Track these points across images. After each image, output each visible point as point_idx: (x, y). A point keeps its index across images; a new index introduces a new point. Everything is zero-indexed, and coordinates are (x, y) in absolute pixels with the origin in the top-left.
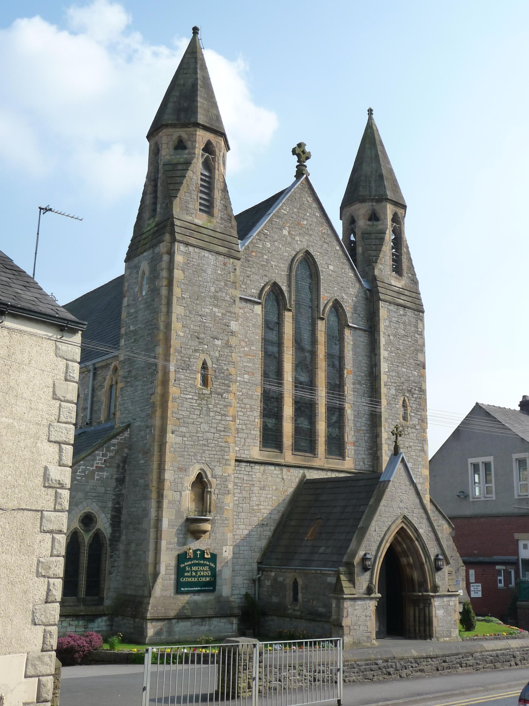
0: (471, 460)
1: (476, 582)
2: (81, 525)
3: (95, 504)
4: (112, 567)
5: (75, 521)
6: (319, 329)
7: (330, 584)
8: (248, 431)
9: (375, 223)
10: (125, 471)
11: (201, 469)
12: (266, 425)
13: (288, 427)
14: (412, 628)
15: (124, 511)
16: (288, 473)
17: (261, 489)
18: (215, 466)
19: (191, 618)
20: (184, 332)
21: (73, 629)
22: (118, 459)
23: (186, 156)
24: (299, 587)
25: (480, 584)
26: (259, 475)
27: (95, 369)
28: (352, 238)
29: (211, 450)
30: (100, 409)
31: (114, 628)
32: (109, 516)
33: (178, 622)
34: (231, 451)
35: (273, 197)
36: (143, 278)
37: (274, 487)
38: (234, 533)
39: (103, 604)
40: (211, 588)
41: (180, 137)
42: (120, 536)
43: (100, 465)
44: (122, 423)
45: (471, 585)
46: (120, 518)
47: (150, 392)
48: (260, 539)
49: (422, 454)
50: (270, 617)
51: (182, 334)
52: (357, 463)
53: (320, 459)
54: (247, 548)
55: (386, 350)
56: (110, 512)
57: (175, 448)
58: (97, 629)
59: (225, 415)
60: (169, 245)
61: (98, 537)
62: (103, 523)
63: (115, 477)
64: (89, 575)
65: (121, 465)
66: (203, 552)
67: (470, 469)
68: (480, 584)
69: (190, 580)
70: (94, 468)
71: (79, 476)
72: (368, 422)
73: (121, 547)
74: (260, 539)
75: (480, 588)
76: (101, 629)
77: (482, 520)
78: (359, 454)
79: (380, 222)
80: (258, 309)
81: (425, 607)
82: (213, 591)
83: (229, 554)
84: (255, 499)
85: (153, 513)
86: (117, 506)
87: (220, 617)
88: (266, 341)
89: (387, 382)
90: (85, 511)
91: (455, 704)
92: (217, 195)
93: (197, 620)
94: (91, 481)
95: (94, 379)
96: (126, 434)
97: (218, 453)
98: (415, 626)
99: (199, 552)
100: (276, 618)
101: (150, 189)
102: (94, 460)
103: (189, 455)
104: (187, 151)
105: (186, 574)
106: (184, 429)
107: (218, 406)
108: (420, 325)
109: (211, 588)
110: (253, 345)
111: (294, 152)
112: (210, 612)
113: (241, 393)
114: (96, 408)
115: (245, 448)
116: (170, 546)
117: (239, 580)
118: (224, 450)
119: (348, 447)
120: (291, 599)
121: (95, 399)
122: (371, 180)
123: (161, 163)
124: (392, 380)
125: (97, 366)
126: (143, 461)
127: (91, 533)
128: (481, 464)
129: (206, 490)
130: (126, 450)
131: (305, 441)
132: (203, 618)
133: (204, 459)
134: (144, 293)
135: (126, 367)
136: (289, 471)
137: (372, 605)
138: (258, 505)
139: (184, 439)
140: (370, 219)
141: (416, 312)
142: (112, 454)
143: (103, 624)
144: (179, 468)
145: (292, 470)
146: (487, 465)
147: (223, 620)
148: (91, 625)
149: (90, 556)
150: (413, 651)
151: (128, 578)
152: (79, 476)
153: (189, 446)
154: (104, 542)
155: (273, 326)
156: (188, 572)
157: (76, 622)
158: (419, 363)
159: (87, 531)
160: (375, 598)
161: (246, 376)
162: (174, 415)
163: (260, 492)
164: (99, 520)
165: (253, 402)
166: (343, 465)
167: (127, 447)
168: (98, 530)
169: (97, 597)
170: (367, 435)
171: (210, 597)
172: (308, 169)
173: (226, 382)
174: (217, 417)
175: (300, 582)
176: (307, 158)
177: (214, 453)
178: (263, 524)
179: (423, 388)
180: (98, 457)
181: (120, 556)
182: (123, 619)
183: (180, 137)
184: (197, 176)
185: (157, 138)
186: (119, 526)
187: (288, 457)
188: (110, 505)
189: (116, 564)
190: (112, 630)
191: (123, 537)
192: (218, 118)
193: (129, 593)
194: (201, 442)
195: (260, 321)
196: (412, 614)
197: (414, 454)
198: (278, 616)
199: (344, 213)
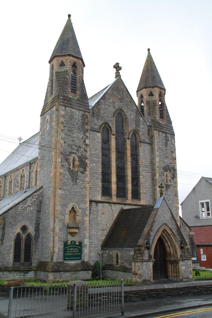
0: (200, 202)
1: (203, 254)
2: (21, 230)
3: (28, 222)
4: (36, 249)
5: (18, 229)
6: (127, 143)
7: (132, 255)
8: (96, 189)
9: (152, 97)
10: (41, 207)
11: (73, 205)
12: (104, 186)
13: (114, 187)
14: (170, 275)
15: (41, 225)
16: (114, 207)
17: (102, 214)
18: (80, 204)
19: (70, 271)
20: (65, 145)
21: (18, 276)
22: (37, 202)
23: (65, 69)
24: (119, 257)
25: (205, 255)
26: (101, 208)
27: (30, 164)
28: (142, 104)
29: (78, 197)
30: (32, 181)
31: (37, 276)
32: (34, 227)
33: (64, 273)
34: (87, 197)
35: (84, 64)
36: (47, 122)
37: (108, 213)
38: (90, 233)
39: (32, 265)
40: (79, 258)
41: (62, 61)
42: (39, 236)
43: (29, 204)
44: (40, 186)
45: (202, 255)
46: (39, 228)
47: (50, 172)
48: (102, 236)
49: (175, 197)
50: (107, 271)
51: (64, 146)
52: (146, 202)
53: (129, 200)
54: (96, 240)
55: (158, 152)
56: (34, 225)
57: (61, 196)
58: (29, 277)
59: (84, 181)
60: (57, 107)
61: (29, 236)
62: (31, 230)
63: (36, 209)
64: (25, 253)
65: (39, 204)
66: (75, 242)
67: (200, 206)
68: (205, 255)
69: (69, 254)
70: (27, 206)
71: (20, 209)
72: (151, 184)
73: (40, 240)
74: (102, 236)
75: (205, 257)
76: (31, 277)
77: (206, 227)
78: (147, 198)
79: (154, 97)
80: (99, 135)
81: (176, 265)
82: (80, 259)
83: (87, 243)
84: (99, 218)
85: (52, 225)
86: (38, 222)
87: (84, 270)
88: (103, 149)
89: (159, 166)
90: (23, 224)
91: (164, 317)
92: (78, 85)
93: (73, 272)
94: (25, 211)
95: (30, 168)
96: (41, 191)
97: (81, 198)
98: (172, 274)
99: (73, 242)
100: (109, 271)
101: (50, 84)
102: (26, 202)
103: (68, 199)
104: (65, 67)
105: (67, 252)
106: (65, 188)
107: (81, 177)
108: (173, 141)
109: (79, 258)
110: (97, 150)
111: (115, 67)
112: (79, 269)
113: (92, 172)
114: (31, 181)
115: (94, 196)
116: (60, 239)
117: (93, 254)
118: (84, 196)
119: (141, 195)
120: (116, 262)
121: (31, 177)
122: (151, 78)
123: (54, 72)
124: (161, 165)
125: (31, 162)
126: (47, 202)
127: (26, 234)
128: (204, 203)
129: (76, 214)
130: (41, 198)
131: (121, 192)
132: (76, 271)
133: (75, 200)
134: (48, 129)
135: (41, 161)
136: (115, 206)
137: (151, 264)
138: (100, 221)
139: (66, 192)
140: (149, 96)
141: (171, 135)
142: (35, 200)
143: (32, 274)
144: (63, 205)
145: (116, 205)
146: (207, 203)
147: (85, 272)
148: (26, 275)
149: (26, 244)
150: (165, 286)
151: (43, 254)
152: (20, 209)
153: (68, 195)
154: (32, 238)
155: (106, 142)
156: (68, 251)
157: (20, 274)
158: (173, 157)
159: (24, 233)
160: (153, 261)
161: (94, 164)
162: (61, 181)
163: (102, 215)
164: (29, 228)
165: (97, 176)
166: (139, 203)
167: (41, 197)
168: (29, 233)
169: (29, 263)
170: (151, 189)
171: (79, 262)
172: (121, 74)
173: (84, 167)
174: (80, 182)
175: (119, 255)
176: (120, 69)
177: (79, 198)
178: (103, 230)
179: (175, 168)
180: (28, 201)
181: (39, 244)
182: (40, 272)
183: (62, 61)
184: (70, 77)
185: (53, 62)
186: (38, 231)
187: (114, 199)
188: (34, 222)
189: (37, 248)
190: (36, 277)
191: (41, 236)
192: (79, 52)
193: (43, 260)
194: (73, 193)
195: (100, 139)
196: (170, 269)
197: (172, 197)
198: (110, 270)
199: (138, 94)
